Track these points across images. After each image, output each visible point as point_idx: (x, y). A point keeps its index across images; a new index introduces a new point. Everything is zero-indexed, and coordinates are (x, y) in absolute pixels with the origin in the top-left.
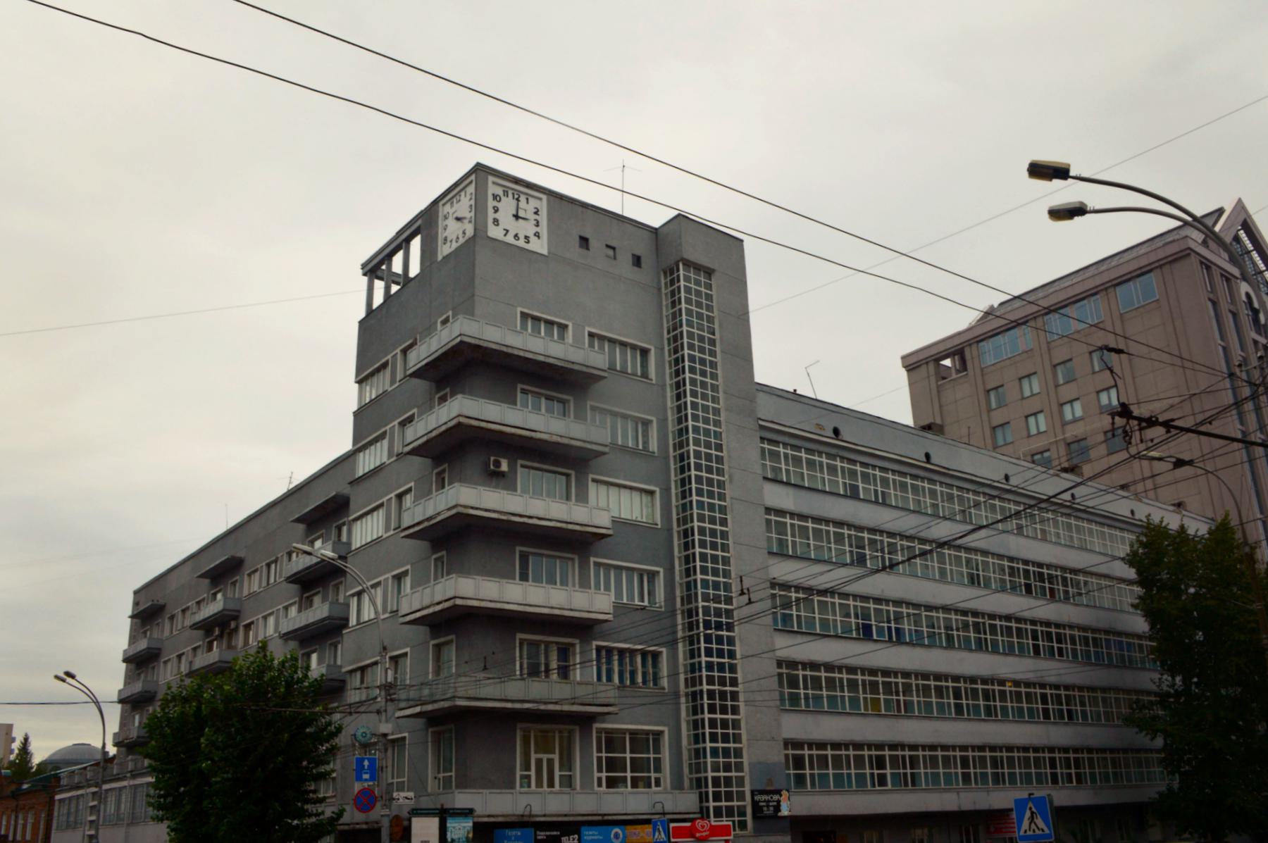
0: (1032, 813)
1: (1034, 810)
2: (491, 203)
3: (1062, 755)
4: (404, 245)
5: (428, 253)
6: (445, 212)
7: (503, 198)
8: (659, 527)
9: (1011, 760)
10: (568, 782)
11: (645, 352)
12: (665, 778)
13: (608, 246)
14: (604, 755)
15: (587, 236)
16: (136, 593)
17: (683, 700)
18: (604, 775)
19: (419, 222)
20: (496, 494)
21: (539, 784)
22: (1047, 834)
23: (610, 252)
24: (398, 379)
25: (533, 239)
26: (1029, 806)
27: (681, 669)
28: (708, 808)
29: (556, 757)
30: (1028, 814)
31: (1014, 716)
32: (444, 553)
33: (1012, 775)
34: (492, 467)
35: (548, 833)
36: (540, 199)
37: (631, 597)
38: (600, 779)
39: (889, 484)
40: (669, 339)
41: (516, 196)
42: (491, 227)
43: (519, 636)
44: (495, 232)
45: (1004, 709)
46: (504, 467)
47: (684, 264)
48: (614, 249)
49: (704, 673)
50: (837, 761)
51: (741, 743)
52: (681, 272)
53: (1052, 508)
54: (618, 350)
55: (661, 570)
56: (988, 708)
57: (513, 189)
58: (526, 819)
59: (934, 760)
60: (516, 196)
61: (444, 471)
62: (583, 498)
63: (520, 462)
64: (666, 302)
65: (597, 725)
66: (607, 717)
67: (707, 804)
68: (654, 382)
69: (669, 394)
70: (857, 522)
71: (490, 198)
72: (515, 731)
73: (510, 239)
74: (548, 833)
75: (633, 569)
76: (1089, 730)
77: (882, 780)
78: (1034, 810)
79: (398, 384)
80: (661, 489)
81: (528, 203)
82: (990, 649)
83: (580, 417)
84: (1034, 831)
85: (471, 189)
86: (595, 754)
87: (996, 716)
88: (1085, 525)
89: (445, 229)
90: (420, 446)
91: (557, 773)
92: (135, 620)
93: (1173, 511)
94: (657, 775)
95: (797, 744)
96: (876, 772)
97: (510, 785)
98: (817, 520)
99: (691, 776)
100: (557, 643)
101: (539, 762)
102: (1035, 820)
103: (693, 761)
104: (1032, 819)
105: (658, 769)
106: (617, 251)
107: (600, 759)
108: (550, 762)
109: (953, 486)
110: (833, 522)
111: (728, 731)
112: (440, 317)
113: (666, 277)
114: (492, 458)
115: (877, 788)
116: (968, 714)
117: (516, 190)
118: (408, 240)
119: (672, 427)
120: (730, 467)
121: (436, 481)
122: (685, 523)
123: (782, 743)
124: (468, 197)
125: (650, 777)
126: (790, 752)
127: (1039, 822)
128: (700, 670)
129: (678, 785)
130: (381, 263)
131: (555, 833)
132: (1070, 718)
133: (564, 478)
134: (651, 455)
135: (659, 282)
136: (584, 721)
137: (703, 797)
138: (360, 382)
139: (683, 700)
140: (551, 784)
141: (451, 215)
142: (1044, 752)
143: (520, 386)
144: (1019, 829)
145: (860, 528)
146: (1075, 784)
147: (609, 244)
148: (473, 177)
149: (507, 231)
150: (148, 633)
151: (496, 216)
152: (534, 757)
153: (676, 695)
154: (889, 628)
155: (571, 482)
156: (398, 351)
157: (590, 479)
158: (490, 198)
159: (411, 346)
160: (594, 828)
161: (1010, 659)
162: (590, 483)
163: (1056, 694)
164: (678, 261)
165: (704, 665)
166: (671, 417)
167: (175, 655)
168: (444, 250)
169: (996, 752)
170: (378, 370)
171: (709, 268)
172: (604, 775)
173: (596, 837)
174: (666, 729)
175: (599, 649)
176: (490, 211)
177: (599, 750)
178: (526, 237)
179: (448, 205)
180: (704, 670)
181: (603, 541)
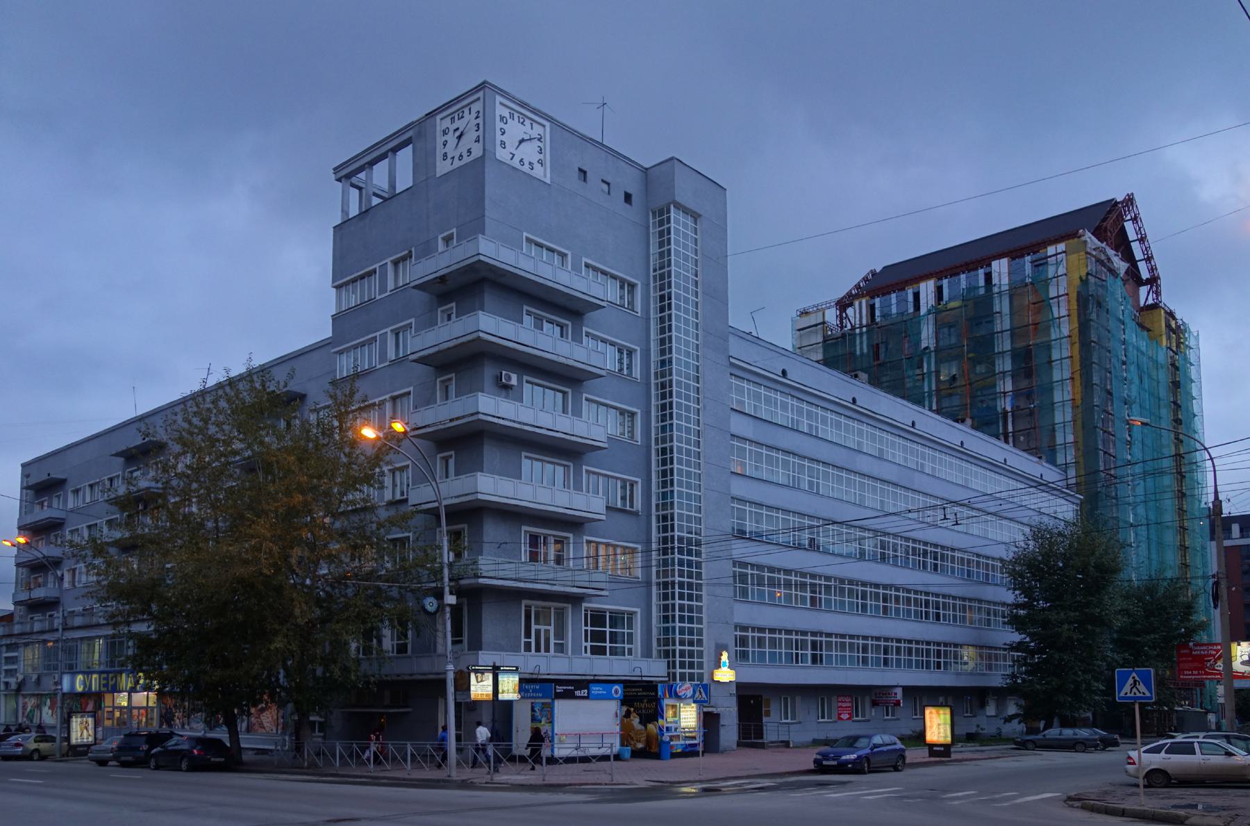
0: (1135, 681)
1: (1137, 678)
2: (499, 125)
6: (444, 128)
8: (639, 443)
9: (898, 649)
10: (560, 648)
11: (632, 286)
12: (636, 649)
13: (603, 181)
14: (589, 628)
15: (584, 168)
17: (654, 588)
18: (589, 644)
21: (538, 650)
23: (605, 187)
25: (537, 166)
29: (552, 628)
30: (1131, 681)
31: (903, 616)
33: (898, 661)
34: (504, 380)
35: (565, 688)
36: (544, 126)
37: (625, 505)
38: (586, 647)
39: (787, 408)
40: (655, 277)
41: (522, 120)
42: (499, 150)
43: (524, 528)
44: (502, 155)
45: (897, 610)
46: (514, 381)
48: (608, 184)
50: (773, 643)
51: (702, 624)
53: (1062, 496)
55: (639, 480)
56: (885, 608)
58: (535, 676)
59: (761, 642)
60: (522, 120)
61: (450, 379)
62: (577, 413)
63: (525, 378)
64: (654, 241)
65: (584, 605)
66: (593, 598)
68: (639, 315)
71: (498, 119)
73: (516, 163)
74: (565, 688)
75: (617, 478)
76: (950, 629)
77: (886, 662)
78: (1137, 678)
79: (388, 293)
83: (577, 338)
84: (1135, 694)
86: (584, 628)
89: (445, 145)
90: (430, 355)
91: (552, 641)
93: (1036, 462)
94: (630, 646)
96: (800, 652)
97: (516, 649)
98: (769, 447)
99: (659, 648)
100: (554, 536)
101: (538, 632)
102: (1137, 686)
103: (662, 637)
105: (630, 641)
106: (611, 186)
107: (586, 631)
108: (547, 632)
109: (744, 379)
110: (766, 446)
111: (691, 616)
113: (654, 217)
114: (504, 372)
116: (871, 612)
118: (395, 150)
119: (654, 357)
121: (440, 389)
124: (474, 115)
125: (624, 647)
127: (1142, 688)
129: (647, 654)
131: (570, 688)
134: (635, 381)
135: (648, 222)
136: (575, 600)
137: (671, 665)
139: (654, 588)
140: (547, 650)
142: (892, 642)
147: (605, 179)
148: (480, 94)
149: (514, 155)
151: (503, 138)
152: (534, 627)
154: (919, 560)
156: (388, 261)
158: (498, 119)
161: (907, 571)
164: (670, 203)
165: (676, 561)
166: (654, 347)
168: (443, 168)
170: (362, 277)
171: (695, 212)
172: (589, 644)
173: (600, 692)
174: (638, 610)
175: (589, 542)
176: (498, 133)
177: (586, 625)
178: (530, 163)
181: (594, 453)
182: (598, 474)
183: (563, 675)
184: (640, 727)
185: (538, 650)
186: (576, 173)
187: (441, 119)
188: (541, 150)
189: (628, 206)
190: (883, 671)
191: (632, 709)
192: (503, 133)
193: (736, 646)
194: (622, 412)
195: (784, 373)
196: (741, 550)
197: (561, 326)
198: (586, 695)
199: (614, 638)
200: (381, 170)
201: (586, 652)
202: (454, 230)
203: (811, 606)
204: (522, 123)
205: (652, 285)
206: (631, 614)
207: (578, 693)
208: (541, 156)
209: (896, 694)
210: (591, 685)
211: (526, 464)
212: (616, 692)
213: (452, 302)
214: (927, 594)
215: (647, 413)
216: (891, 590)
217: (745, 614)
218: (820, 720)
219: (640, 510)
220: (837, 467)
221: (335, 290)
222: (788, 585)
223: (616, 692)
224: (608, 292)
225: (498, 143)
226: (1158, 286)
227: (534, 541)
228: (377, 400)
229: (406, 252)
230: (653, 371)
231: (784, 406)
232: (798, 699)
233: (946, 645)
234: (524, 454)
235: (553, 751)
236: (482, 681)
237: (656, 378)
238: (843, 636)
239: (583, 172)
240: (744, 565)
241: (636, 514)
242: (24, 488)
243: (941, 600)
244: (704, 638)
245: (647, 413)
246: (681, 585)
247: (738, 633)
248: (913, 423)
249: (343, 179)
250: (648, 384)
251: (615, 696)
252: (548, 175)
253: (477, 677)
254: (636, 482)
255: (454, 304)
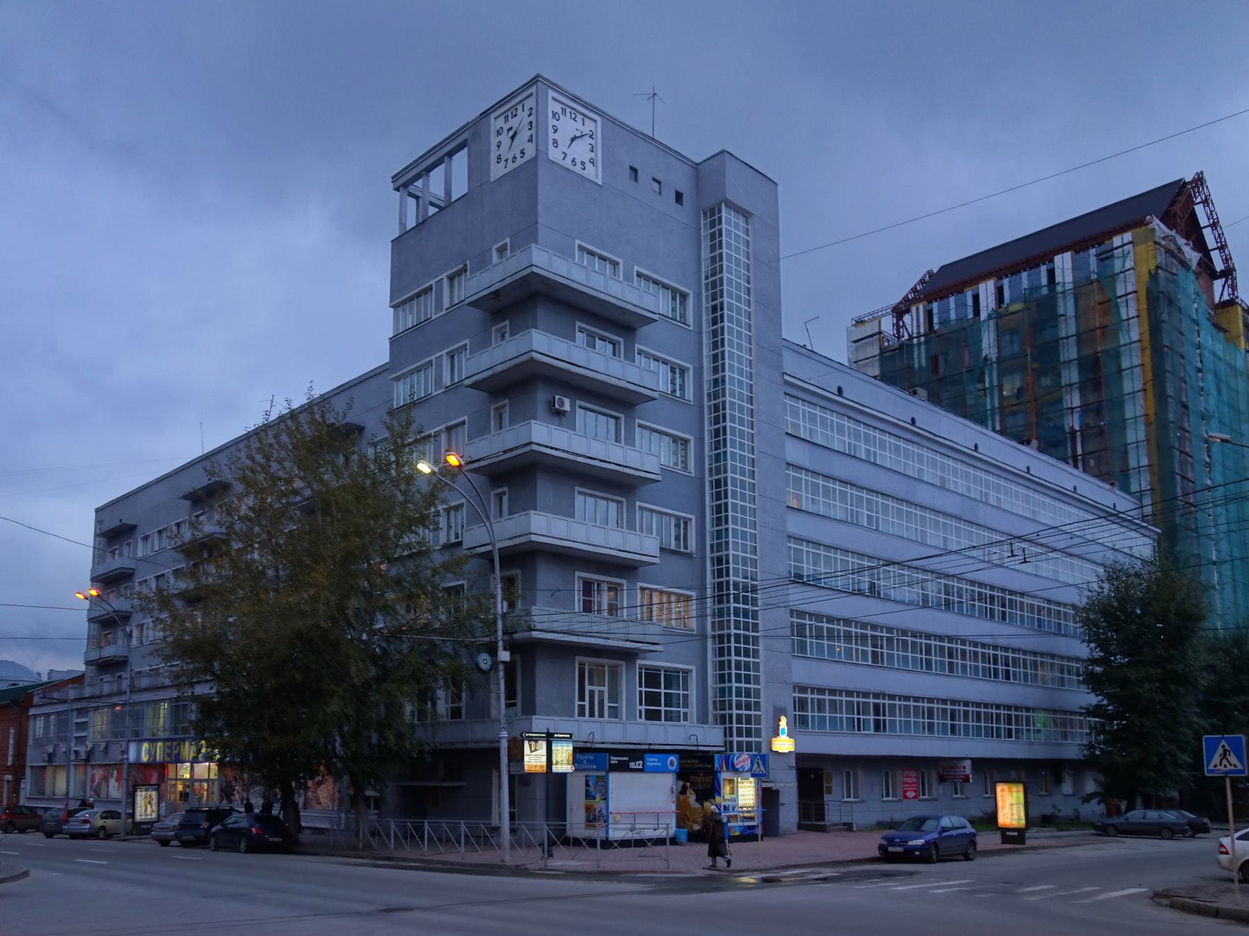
0: (1225, 751)
1: (1227, 747)
3: (940, 706)
4: (446, 158)
5: (477, 170)
6: (498, 128)
7: (562, 117)
8: (693, 475)
9: (966, 713)
10: (615, 712)
13: (655, 180)
14: (644, 689)
16: (98, 511)
17: (710, 641)
18: (644, 707)
19: (466, 135)
20: (546, 429)
21: (592, 715)
22: (1240, 770)
23: (656, 186)
24: (444, 308)
25: (589, 165)
26: (1222, 744)
27: (709, 612)
28: (731, 742)
29: (605, 689)
30: (1220, 751)
32: (505, 489)
34: (557, 406)
35: (620, 758)
36: (595, 121)
38: (640, 711)
40: (707, 285)
41: (573, 116)
43: (578, 574)
46: (567, 407)
47: (726, 206)
48: (659, 183)
49: (732, 618)
50: (834, 706)
52: (724, 214)
54: (661, 292)
55: (693, 517)
57: (582, 114)
58: (588, 745)
60: (573, 116)
61: (504, 406)
63: (579, 402)
64: (705, 244)
65: (639, 662)
67: (731, 739)
69: (706, 341)
70: (857, 483)
72: (575, 660)
73: (567, 163)
74: (620, 758)
78: (1227, 747)
79: (444, 312)
80: (695, 438)
81: (584, 125)
82: (956, 611)
83: (630, 357)
85: (530, 103)
87: (882, 663)
88: (837, 487)
89: (499, 146)
91: (606, 704)
92: (98, 539)
94: (685, 710)
95: (803, 689)
98: (827, 477)
100: (608, 582)
101: (592, 692)
102: (1228, 757)
103: (718, 699)
104: (1224, 755)
105: (686, 705)
106: (662, 184)
107: (641, 692)
108: (601, 693)
112: (496, 243)
113: (705, 219)
114: (557, 397)
115: (862, 732)
117: (573, 109)
118: (450, 154)
119: (707, 376)
120: (758, 420)
121: (494, 417)
122: (718, 472)
123: (792, 687)
124: (526, 112)
126: (797, 695)
127: (1233, 759)
128: (729, 615)
129: (703, 719)
130: (417, 177)
131: (625, 759)
132: (951, 670)
133: (612, 421)
136: (629, 656)
137: (728, 732)
138: (395, 307)
139: (710, 641)
140: (601, 715)
141: (505, 131)
143: (578, 324)
144: (1209, 762)
145: (861, 488)
146: (1014, 739)
147: (656, 178)
148: (533, 89)
149: (566, 154)
150: (117, 552)
151: (556, 136)
152: (588, 688)
153: (704, 636)
155: (620, 425)
156: (444, 276)
157: (636, 424)
158: (550, 114)
159: (459, 274)
160: (654, 755)
162: (637, 429)
163: (974, 651)
166: (707, 364)
167: (152, 576)
168: (497, 171)
169: (918, 702)
170: (418, 295)
172: (644, 707)
173: (656, 764)
176: (551, 130)
178: (583, 163)
179: (502, 118)
180: (732, 615)
182: (652, 511)
183: (613, 743)
184: (697, 805)
185: (592, 715)
186: (627, 172)
187: (496, 118)
188: (592, 147)
189: (679, 206)
190: (950, 740)
191: (688, 784)
192: (556, 131)
193: (795, 711)
194: (675, 439)
195: (840, 390)
196: (798, 597)
197: (613, 343)
198: (641, 767)
199: (669, 700)
200: (438, 174)
201: (640, 717)
202: (508, 240)
203: (873, 662)
204: (574, 119)
205: (704, 294)
206: (687, 673)
207: (632, 765)
208: (593, 155)
209: (964, 767)
210: (646, 755)
211: (579, 499)
212: (672, 763)
213: (504, 320)
214: (995, 647)
215: (700, 440)
216: (957, 644)
217: (804, 671)
218: (885, 799)
219: (694, 551)
220: (897, 499)
221: (392, 309)
222: (848, 637)
223: (672, 763)
224: (659, 303)
225: (551, 142)
226: (1234, 279)
227: (588, 587)
228: (432, 432)
229: (461, 266)
230: (706, 392)
231: (841, 430)
232: (860, 773)
233: (1017, 709)
234: (577, 489)
235: (607, 832)
236: (535, 750)
237: (709, 400)
238: (907, 698)
239: (634, 170)
240: (802, 614)
241: (690, 556)
242: (98, 535)
243: (1010, 655)
244: (762, 700)
245: (700, 440)
246: (737, 637)
247: (797, 695)
248: (976, 447)
249: (401, 188)
250: (701, 407)
251: (670, 768)
252: (600, 175)
253: (530, 746)
254: (690, 519)
255: (507, 322)
